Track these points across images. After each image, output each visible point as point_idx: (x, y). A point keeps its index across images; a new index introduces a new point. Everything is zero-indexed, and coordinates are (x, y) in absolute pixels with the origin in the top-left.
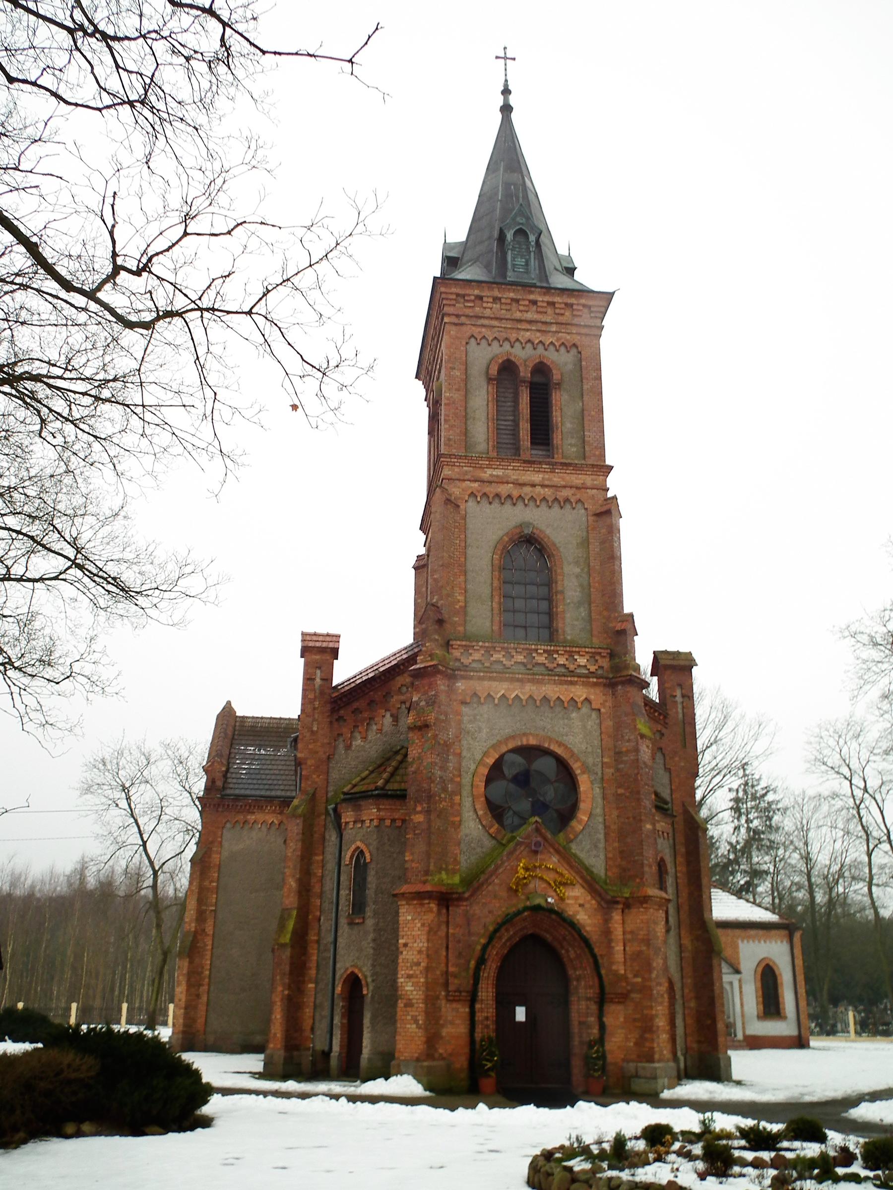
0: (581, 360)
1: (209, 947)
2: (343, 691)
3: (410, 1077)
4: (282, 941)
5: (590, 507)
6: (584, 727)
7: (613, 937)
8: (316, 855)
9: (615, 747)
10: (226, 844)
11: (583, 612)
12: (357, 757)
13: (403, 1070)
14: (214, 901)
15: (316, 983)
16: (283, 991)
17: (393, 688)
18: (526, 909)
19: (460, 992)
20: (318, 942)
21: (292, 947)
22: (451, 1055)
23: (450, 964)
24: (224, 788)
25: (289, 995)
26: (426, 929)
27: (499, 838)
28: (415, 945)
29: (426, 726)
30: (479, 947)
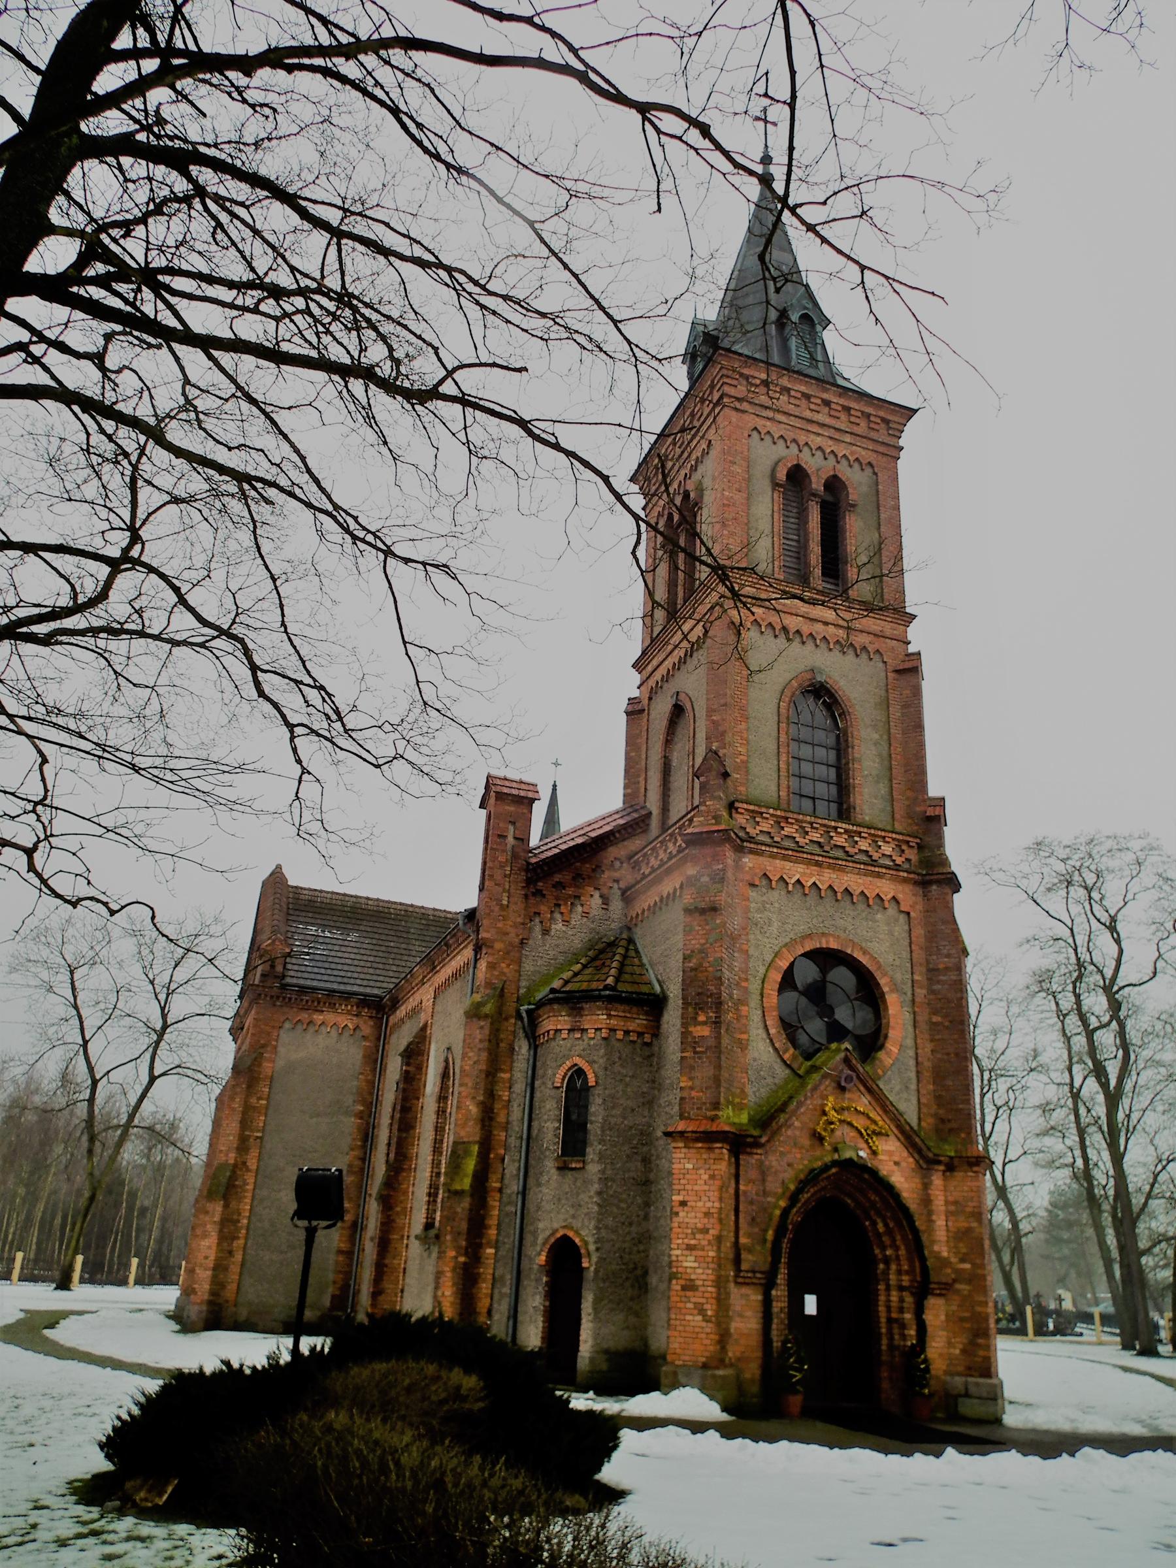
0: (877, 484)
1: (250, 1187)
2: (543, 856)
3: (696, 1392)
4: (457, 1187)
5: (889, 661)
6: (891, 933)
7: (934, 1208)
8: (502, 1070)
9: (928, 962)
10: (282, 1050)
11: (883, 789)
12: (557, 946)
13: (682, 1380)
14: (261, 1124)
15: (497, 1248)
16: (456, 1258)
17: (605, 861)
18: (835, 1163)
19: (754, 1272)
20: (500, 1190)
21: (472, 1195)
22: (739, 1359)
23: (741, 1233)
24: (284, 977)
25: (465, 1263)
26: (718, 1183)
27: (795, 1066)
28: (700, 1204)
29: (714, 909)
30: (778, 1212)
